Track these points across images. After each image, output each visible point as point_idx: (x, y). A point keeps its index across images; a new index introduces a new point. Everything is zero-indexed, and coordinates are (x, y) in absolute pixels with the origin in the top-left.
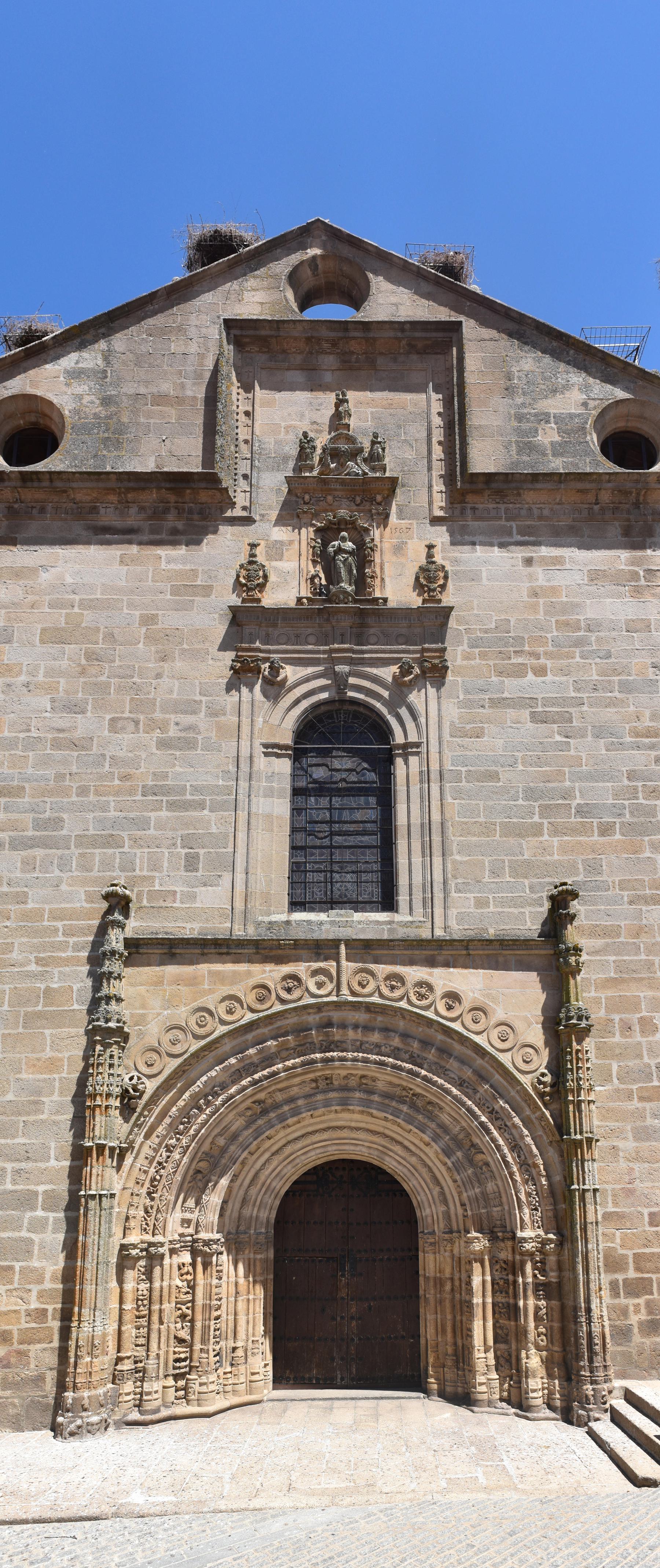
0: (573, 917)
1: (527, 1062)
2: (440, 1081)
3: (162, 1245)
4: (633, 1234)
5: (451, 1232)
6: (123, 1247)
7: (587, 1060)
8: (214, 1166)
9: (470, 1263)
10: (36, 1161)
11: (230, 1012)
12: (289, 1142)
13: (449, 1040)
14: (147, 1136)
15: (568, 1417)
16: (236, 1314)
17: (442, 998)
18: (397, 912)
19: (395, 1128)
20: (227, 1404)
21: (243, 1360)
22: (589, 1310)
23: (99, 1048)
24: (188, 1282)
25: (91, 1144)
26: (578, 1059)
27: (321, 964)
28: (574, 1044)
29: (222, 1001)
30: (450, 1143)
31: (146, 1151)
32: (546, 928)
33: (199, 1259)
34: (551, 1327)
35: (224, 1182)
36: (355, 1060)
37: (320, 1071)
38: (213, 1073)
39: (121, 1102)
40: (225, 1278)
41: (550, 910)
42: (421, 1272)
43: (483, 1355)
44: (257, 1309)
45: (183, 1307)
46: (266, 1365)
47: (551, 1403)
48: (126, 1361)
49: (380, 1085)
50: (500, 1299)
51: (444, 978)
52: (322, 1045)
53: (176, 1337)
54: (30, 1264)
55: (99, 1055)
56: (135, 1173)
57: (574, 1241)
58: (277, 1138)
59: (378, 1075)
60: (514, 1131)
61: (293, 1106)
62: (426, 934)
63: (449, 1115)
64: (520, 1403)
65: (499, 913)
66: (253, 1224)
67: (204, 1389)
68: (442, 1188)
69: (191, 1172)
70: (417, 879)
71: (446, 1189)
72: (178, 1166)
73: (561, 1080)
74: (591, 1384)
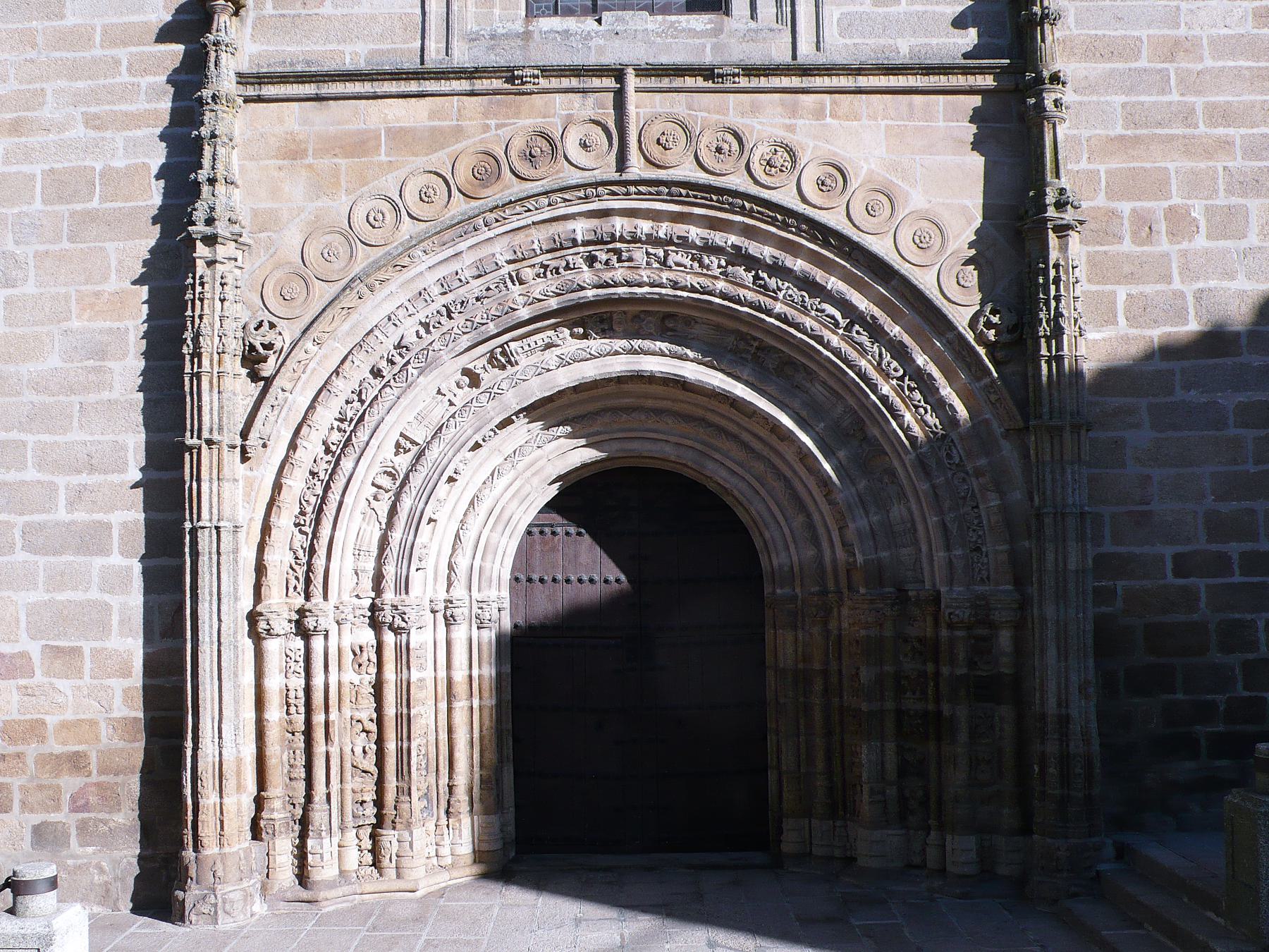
10: (105, 472)
18: (727, 13)
68: (809, 516)
71: (816, 516)
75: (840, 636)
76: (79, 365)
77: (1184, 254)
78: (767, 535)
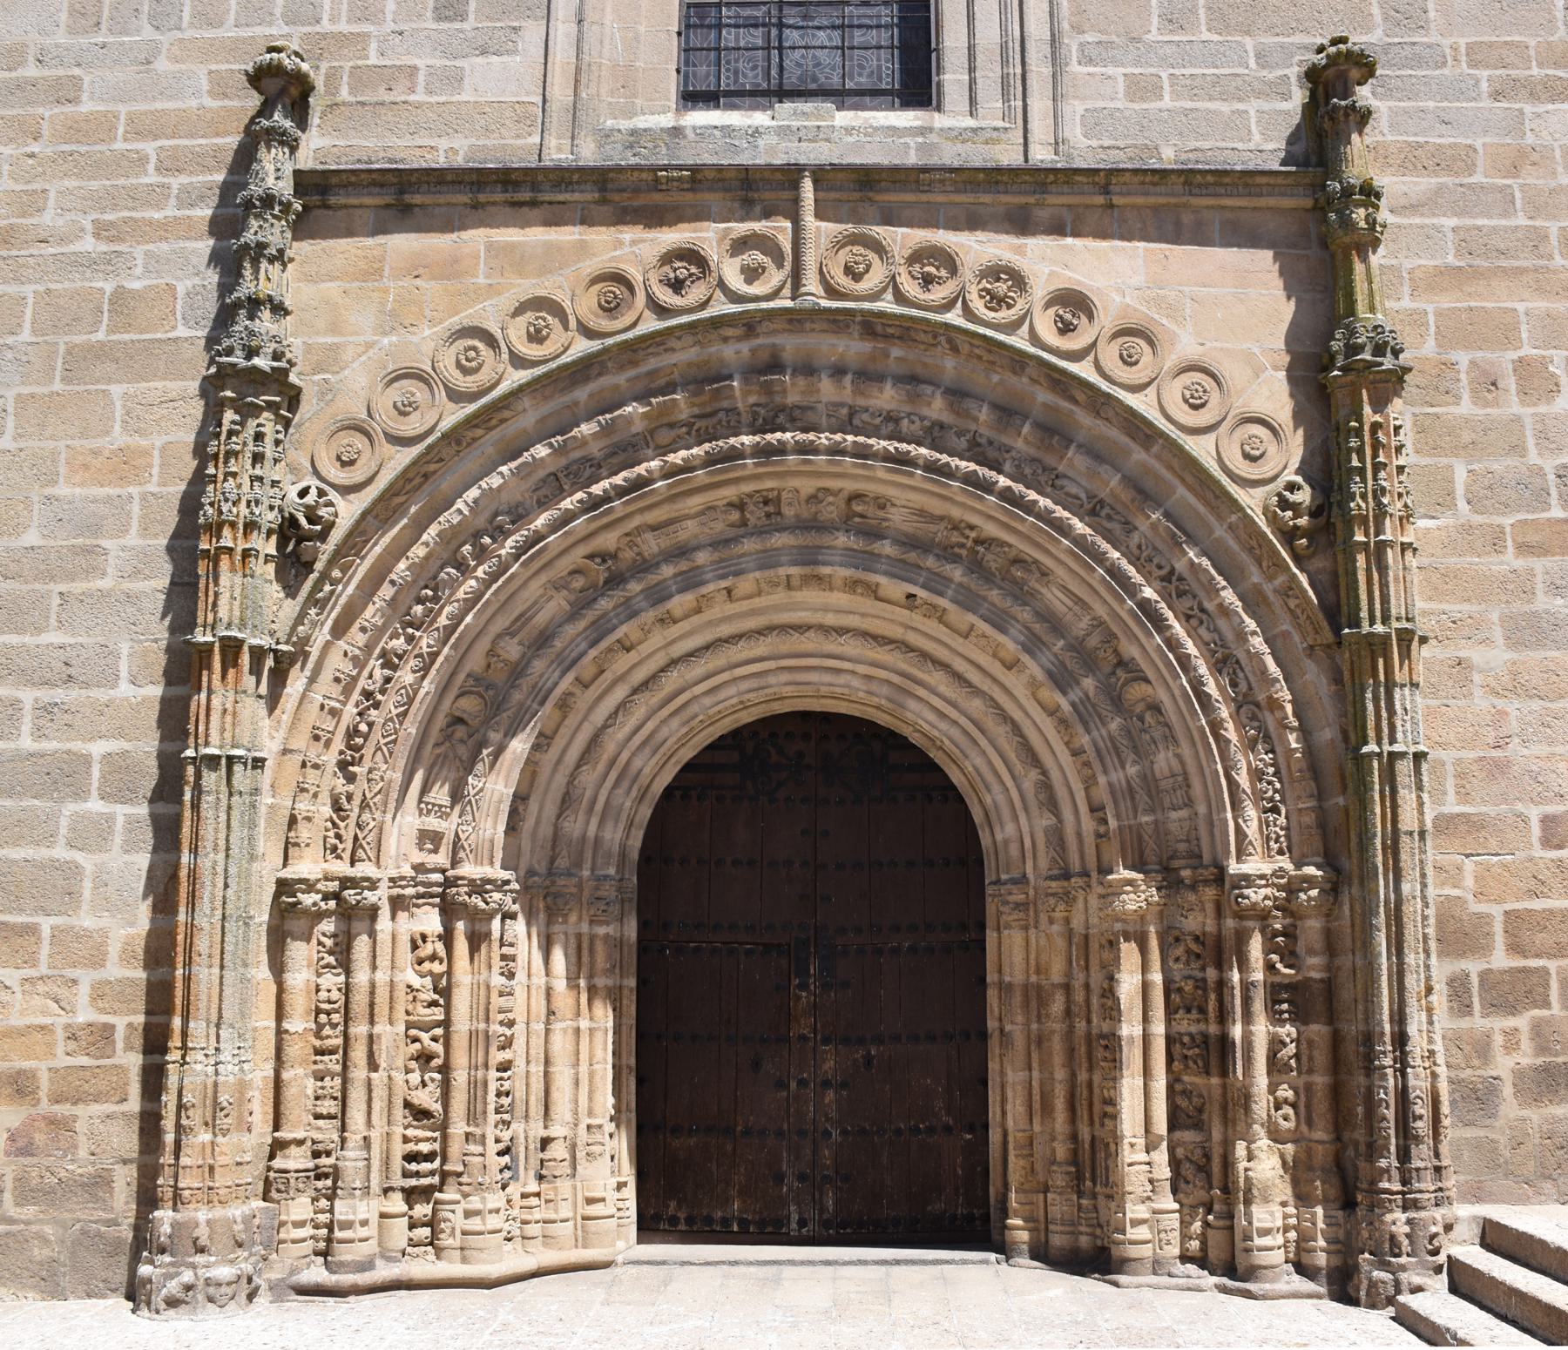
0: (1363, 117)
1: (1254, 459)
2: (1044, 502)
3: (373, 884)
4: (1504, 865)
5: (1066, 876)
6: (284, 887)
7: (1399, 449)
8: (494, 707)
9: (1113, 945)
11: (536, 337)
12: (674, 662)
13: (1065, 405)
14: (339, 630)
15: (1344, 1287)
16: (547, 1062)
17: (1048, 305)
18: (939, 109)
19: (932, 627)
20: (529, 1263)
21: (565, 1168)
22: (1401, 1039)
23: (229, 416)
24: (436, 978)
25: (209, 638)
26: (1376, 446)
27: (757, 226)
28: (1367, 410)
29: (519, 311)
30: (1067, 657)
31: (337, 662)
32: (1299, 149)
33: (460, 926)
34: (1309, 1087)
35: (519, 746)
36: (836, 450)
37: (751, 479)
38: (495, 481)
39: (281, 546)
40: (521, 976)
41: (1305, 107)
42: (991, 977)
43: (1143, 1157)
44: (599, 1053)
45: (425, 1037)
46: (620, 1186)
47: (1306, 1259)
48: (293, 1150)
49: (897, 518)
50: (1187, 1025)
51: (1049, 261)
52: (755, 415)
53: (407, 1104)
54: (74, 921)
55: (231, 433)
56: (312, 715)
57: (1367, 875)
58: (645, 648)
59: (891, 492)
60: (1222, 623)
61: (684, 566)
62: (1009, 156)
63: (1065, 589)
64: (1228, 1262)
65: (1186, 112)
66: (588, 855)
67: (475, 1224)
68: (1044, 773)
69: (441, 721)
70: (989, 34)
71: (1055, 775)
72: (411, 701)
73: (1335, 497)
74: (1405, 1209)
75: (1086, 937)
76: (65, 543)
77: (1542, 419)
78: (988, 800)
